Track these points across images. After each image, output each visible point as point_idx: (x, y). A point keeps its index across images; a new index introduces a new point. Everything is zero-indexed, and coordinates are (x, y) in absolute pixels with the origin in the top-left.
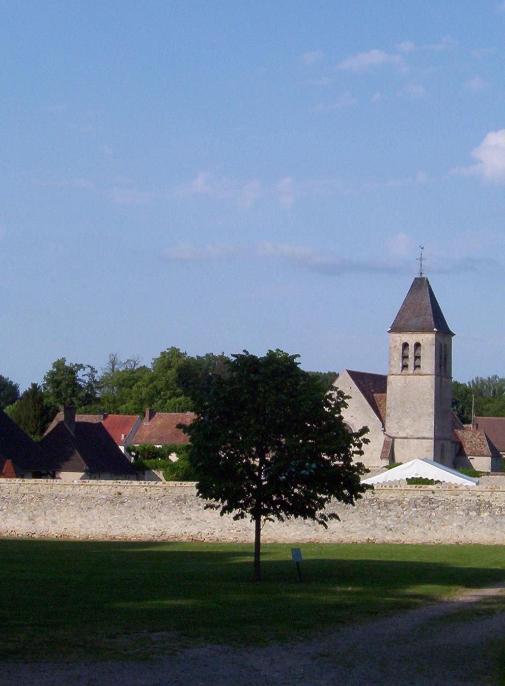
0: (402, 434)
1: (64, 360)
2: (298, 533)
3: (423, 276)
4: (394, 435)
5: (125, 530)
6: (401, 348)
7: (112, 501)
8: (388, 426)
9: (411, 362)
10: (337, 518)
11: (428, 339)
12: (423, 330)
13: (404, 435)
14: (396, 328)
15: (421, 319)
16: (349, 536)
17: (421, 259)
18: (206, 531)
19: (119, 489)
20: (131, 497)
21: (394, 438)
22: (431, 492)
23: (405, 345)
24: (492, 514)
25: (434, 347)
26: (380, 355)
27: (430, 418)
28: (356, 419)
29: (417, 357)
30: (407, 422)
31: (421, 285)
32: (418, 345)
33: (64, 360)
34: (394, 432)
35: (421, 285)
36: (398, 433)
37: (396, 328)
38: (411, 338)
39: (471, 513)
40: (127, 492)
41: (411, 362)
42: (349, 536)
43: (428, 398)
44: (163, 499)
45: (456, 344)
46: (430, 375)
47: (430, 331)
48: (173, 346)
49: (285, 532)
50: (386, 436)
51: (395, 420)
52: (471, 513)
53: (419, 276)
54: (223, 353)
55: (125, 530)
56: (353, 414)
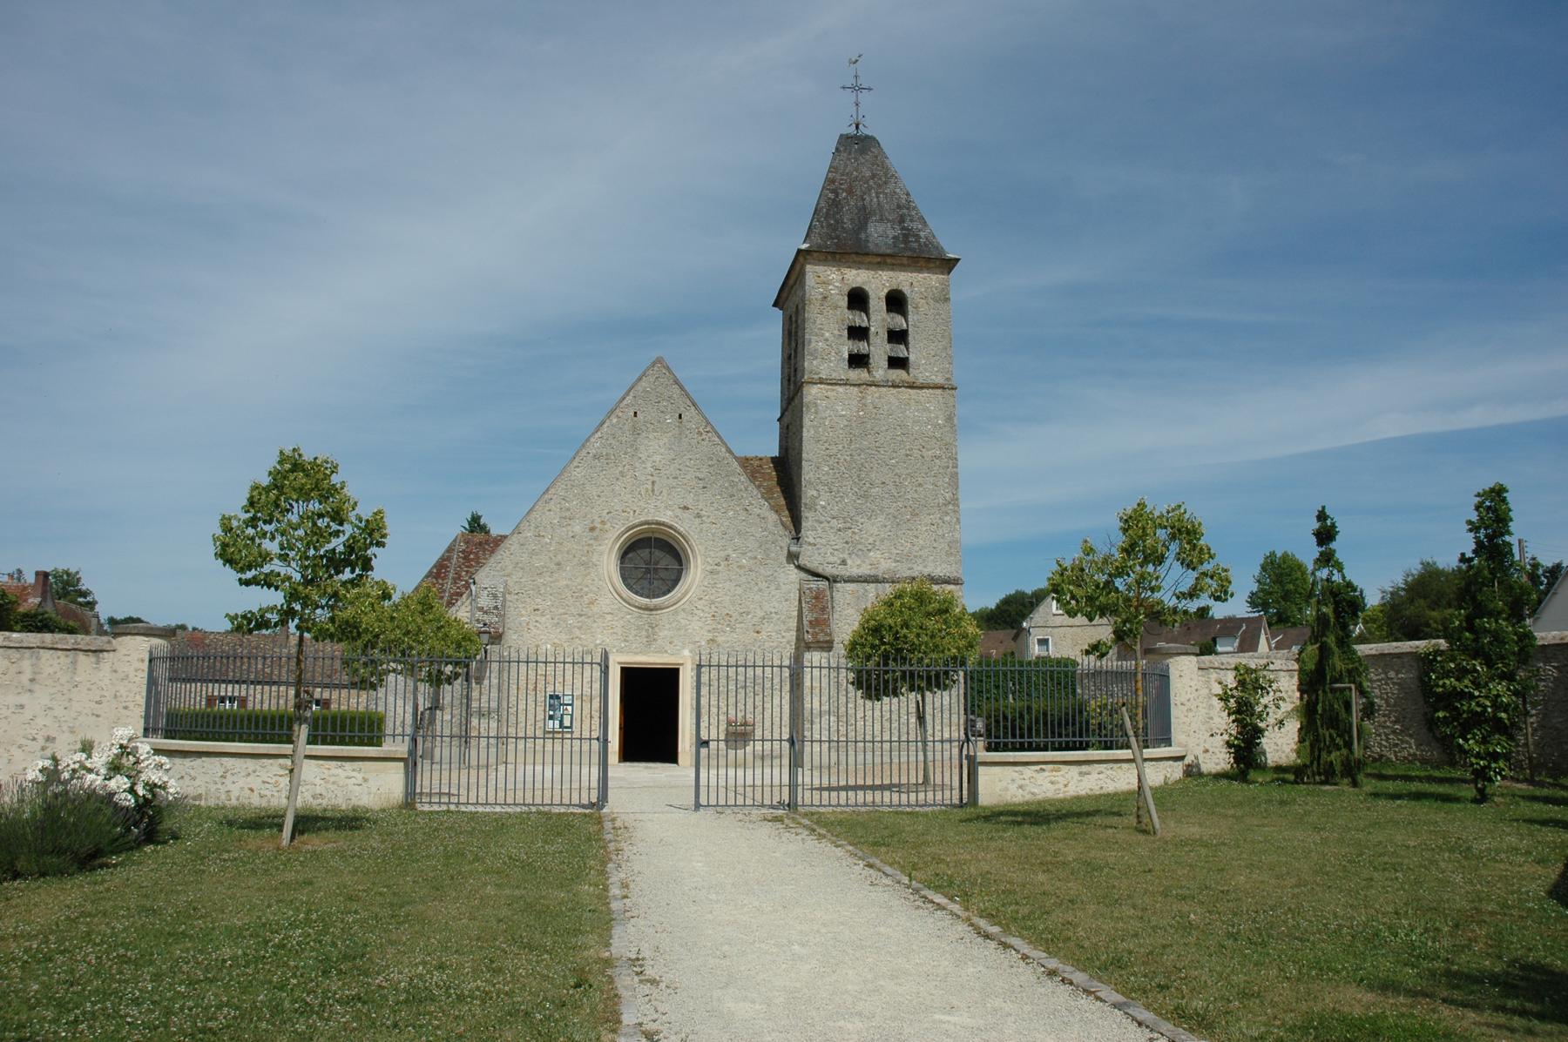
0: (855, 568)
1: (1273, 554)
8: (811, 540)
9: (879, 349)
13: (865, 570)
22: (704, 751)
27: (947, 518)
28: (699, 516)
30: (873, 528)
33: (1273, 554)
34: (831, 559)
36: (844, 562)
41: (879, 349)
43: (938, 457)
46: (936, 387)
50: (803, 575)
51: (834, 523)
53: (852, 130)
54: (1493, 513)
56: (689, 501)
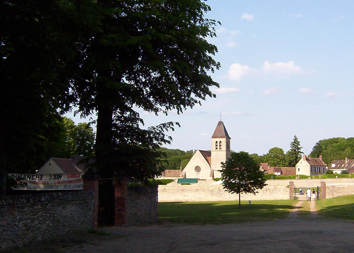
2: (216, 198)
3: (221, 121)
4: (214, 170)
5: (167, 199)
6: (215, 143)
7: (163, 191)
9: (218, 147)
10: (258, 192)
11: (224, 140)
12: (222, 137)
14: (214, 137)
15: (221, 134)
16: (230, 199)
17: (221, 115)
18: (190, 199)
19: (165, 188)
20: (168, 189)
21: (214, 170)
23: (217, 142)
24: (270, 192)
25: (225, 143)
26: (209, 145)
29: (220, 146)
31: (221, 123)
32: (220, 142)
35: (221, 123)
37: (214, 137)
38: (218, 140)
39: (264, 192)
40: (167, 188)
41: (218, 147)
42: (230, 199)
44: (177, 190)
45: (231, 141)
47: (224, 138)
48: (333, 137)
49: (246, 197)
52: (264, 192)
55: (167, 199)
